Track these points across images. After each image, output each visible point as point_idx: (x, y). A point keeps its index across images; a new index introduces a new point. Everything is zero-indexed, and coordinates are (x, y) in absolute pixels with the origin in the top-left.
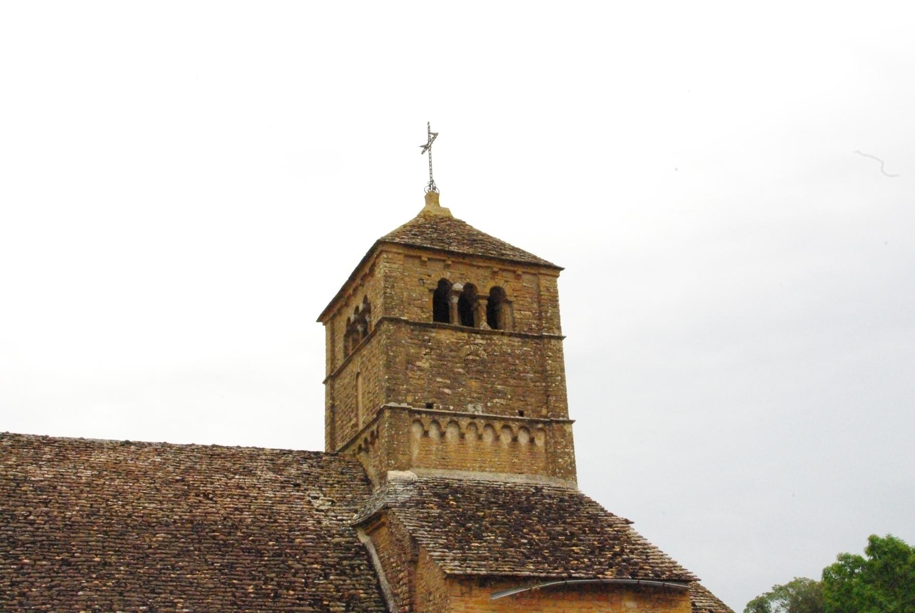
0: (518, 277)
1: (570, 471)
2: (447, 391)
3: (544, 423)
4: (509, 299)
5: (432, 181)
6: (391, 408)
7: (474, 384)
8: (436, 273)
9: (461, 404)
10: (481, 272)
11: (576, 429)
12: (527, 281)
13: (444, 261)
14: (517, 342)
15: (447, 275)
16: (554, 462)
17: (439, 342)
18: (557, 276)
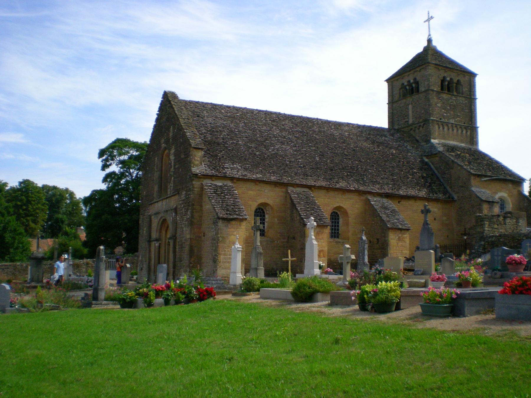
4: (462, 84)
5: (430, 35)
7: (452, 112)
8: (442, 74)
14: (464, 99)
15: (446, 75)
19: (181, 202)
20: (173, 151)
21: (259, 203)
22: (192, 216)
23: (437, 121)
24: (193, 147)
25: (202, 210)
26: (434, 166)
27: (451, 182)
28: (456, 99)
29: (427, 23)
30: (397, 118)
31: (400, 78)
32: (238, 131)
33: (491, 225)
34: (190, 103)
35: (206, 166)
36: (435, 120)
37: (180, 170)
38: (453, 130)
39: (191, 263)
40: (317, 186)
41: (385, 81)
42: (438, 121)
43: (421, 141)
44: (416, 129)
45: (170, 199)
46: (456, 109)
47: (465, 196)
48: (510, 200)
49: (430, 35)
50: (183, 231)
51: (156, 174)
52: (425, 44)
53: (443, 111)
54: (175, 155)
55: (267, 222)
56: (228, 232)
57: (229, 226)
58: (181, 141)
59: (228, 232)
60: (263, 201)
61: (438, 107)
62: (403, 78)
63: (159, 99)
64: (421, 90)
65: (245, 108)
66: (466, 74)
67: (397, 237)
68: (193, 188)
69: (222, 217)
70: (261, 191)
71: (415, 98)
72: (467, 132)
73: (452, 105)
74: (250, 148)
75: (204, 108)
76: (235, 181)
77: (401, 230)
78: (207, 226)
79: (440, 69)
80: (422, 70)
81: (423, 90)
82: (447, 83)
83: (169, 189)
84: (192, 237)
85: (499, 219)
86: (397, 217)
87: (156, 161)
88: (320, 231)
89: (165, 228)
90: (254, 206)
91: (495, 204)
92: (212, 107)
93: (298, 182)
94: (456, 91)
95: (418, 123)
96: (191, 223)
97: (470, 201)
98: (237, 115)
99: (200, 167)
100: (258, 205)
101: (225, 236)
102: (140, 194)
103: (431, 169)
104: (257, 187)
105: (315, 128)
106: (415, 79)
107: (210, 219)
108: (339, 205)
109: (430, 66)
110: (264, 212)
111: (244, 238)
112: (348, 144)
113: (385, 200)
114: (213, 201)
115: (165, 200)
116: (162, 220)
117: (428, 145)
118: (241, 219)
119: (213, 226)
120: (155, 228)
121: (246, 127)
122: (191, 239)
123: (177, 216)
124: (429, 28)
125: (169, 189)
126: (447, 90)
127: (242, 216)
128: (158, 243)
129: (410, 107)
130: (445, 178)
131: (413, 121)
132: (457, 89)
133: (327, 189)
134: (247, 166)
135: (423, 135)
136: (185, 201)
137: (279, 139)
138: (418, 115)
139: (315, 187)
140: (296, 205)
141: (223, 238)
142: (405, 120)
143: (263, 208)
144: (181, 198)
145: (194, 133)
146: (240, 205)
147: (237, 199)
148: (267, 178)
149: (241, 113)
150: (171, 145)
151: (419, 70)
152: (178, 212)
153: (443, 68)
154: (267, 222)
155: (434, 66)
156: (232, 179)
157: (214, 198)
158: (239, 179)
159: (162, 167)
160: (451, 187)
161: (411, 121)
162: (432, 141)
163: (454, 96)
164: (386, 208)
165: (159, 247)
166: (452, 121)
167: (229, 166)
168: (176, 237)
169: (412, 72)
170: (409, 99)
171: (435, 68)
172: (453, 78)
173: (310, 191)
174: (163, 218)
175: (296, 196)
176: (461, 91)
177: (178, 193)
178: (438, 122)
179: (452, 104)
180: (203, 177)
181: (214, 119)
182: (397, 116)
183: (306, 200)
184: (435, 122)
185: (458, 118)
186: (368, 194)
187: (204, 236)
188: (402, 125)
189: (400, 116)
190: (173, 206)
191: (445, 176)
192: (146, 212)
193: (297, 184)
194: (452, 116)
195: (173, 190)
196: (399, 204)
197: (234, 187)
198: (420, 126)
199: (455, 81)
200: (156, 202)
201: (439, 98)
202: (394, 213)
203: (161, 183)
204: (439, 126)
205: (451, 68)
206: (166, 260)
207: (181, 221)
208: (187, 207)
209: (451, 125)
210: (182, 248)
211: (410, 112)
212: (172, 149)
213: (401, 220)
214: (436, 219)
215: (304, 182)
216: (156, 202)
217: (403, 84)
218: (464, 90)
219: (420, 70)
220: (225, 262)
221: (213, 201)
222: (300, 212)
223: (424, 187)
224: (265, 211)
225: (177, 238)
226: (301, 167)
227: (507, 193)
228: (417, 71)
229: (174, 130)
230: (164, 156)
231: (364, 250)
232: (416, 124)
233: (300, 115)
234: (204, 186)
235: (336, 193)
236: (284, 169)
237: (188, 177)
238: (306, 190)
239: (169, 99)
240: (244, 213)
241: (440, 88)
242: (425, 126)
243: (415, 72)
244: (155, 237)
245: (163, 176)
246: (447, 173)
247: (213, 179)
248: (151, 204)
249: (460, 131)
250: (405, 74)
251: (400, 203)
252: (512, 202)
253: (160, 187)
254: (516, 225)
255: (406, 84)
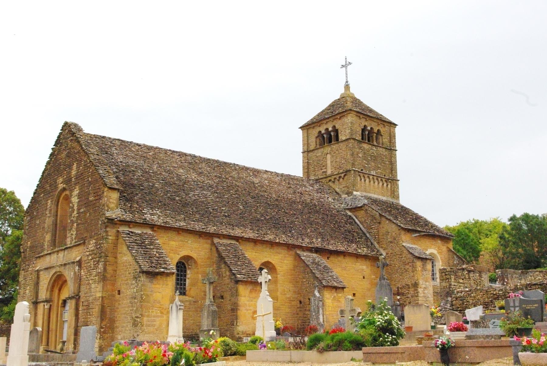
5: (347, 82)
7: (373, 164)
8: (364, 123)
15: (366, 124)
19: (88, 253)
20: (76, 192)
21: (182, 255)
23: (359, 172)
26: (359, 221)
29: (344, 69)
30: (313, 168)
31: (317, 125)
33: (456, 279)
35: (123, 210)
36: (357, 171)
37: (88, 215)
38: (374, 182)
42: (360, 172)
43: (341, 193)
45: (69, 250)
46: (377, 160)
47: (395, 253)
48: (439, 258)
49: (347, 82)
51: (49, 221)
52: (342, 91)
53: (364, 161)
54: (79, 196)
56: (153, 289)
60: (186, 254)
62: (320, 126)
63: (57, 131)
64: (342, 139)
65: (157, 147)
66: (386, 124)
70: (184, 241)
71: (334, 147)
73: (373, 156)
75: (112, 144)
76: (155, 229)
77: (336, 288)
79: (361, 117)
81: (344, 138)
82: (367, 133)
83: (70, 238)
84: (104, 295)
85: (463, 272)
86: (330, 274)
87: (49, 204)
89: (59, 286)
91: (428, 261)
92: (120, 144)
96: (103, 278)
97: (401, 258)
98: (150, 155)
99: (115, 211)
100: (181, 258)
101: (149, 293)
102: (21, 245)
103: (356, 223)
104: (181, 238)
105: (234, 173)
106: (334, 127)
107: (129, 273)
110: (185, 267)
112: (270, 193)
114: (134, 251)
115: (63, 252)
116: (55, 276)
118: (167, 273)
119: (134, 282)
120: (46, 286)
121: (161, 168)
123: (81, 270)
125: (70, 238)
126: (367, 140)
127: (169, 269)
128: (49, 305)
129: (329, 156)
130: (371, 232)
131: (332, 172)
132: (377, 139)
133: (255, 242)
134: (168, 212)
135: (343, 187)
136: (95, 252)
137: (199, 184)
138: (337, 165)
139: (243, 239)
140: (225, 258)
141: (147, 296)
142: (323, 171)
143: (184, 262)
145: (107, 172)
147: (160, 250)
148: (192, 227)
149: (154, 153)
151: (339, 118)
152: (83, 266)
153: (364, 117)
154: (188, 278)
155: (355, 113)
156: (152, 226)
157: (134, 248)
158: (160, 227)
159: (57, 212)
160: (378, 243)
161: (329, 172)
162: (355, 193)
163: (374, 147)
164: (318, 264)
165: (50, 309)
166: (373, 173)
167: (148, 211)
168: (80, 297)
169: (331, 119)
170: (327, 149)
172: (373, 128)
173: (238, 243)
174: (58, 273)
175: (224, 248)
176: (381, 142)
177: (84, 243)
178: (359, 174)
179: (372, 154)
180: (120, 223)
182: (312, 166)
183: (235, 253)
184: (357, 173)
185: (379, 170)
186: (298, 248)
187: (119, 294)
188: (319, 176)
189: (317, 166)
190: (76, 258)
191: (372, 231)
192: (31, 266)
194: (373, 168)
195: (75, 238)
196: (328, 260)
197: (155, 236)
198: (340, 177)
199: (376, 131)
202: (326, 270)
203: (56, 231)
205: (372, 117)
206: (58, 326)
207: (88, 276)
209: (372, 177)
211: (329, 162)
212: (75, 190)
213: (335, 278)
214: (365, 277)
215: (232, 233)
217: (320, 132)
218: (384, 141)
220: (149, 326)
221: (134, 251)
222: (231, 267)
224: (187, 266)
226: (226, 216)
228: (337, 118)
230: (61, 198)
231: (318, 308)
233: (216, 159)
234: (122, 233)
236: (208, 217)
237: (100, 223)
238: (233, 242)
241: (361, 138)
242: (346, 177)
243: (334, 120)
244: (44, 297)
248: (39, 257)
249: (381, 184)
252: (442, 259)
253: (54, 236)
254: (479, 279)
255: (323, 132)
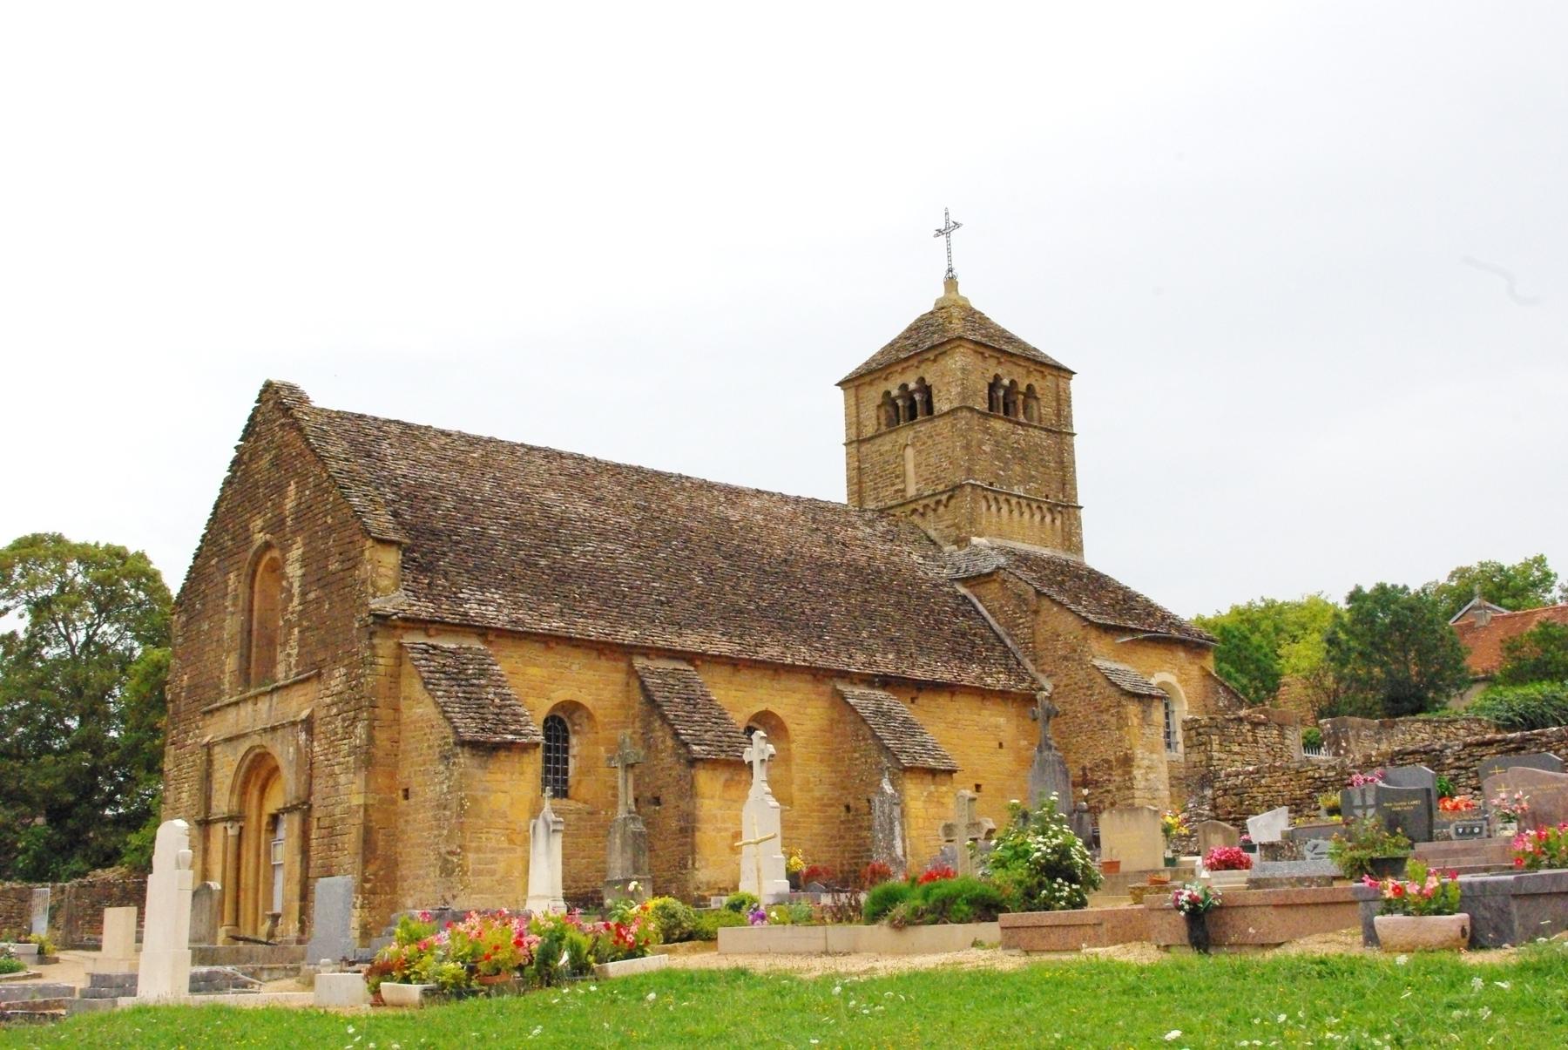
0: (1044, 377)
1: (1079, 549)
2: (1001, 473)
3: (1063, 506)
4: (1039, 396)
5: (950, 270)
6: (972, 485)
7: (1018, 468)
8: (993, 369)
9: (1010, 486)
10: (1020, 370)
11: (1083, 514)
12: (1050, 381)
13: (998, 358)
14: (1043, 434)
15: (999, 371)
16: (1069, 540)
17: (995, 430)
18: (1070, 379)
19: (328, 700)
20: (296, 552)
22: (371, 739)
23: (984, 489)
24: (373, 538)
25: (397, 721)
26: (986, 607)
27: (1034, 648)
28: (1026, 435)
32: (481, 501)
34: (342, 418)
35: (411, 594)
36: (979, 486)
37: (327, 607)
38: (1022, 514)
39: (366, 880)
40: (709, 655)
41: (838, 385)
42: (987, 489)
43: (941, 543)
44: (929, 510)
47: (1076, 684)
49: (950, 270)
50: (337, 784)
51: (232, 625)
52: (940, 292)
54: (305, 561)
55: (574, 756)
56: (488, 784)
57: (491, 767)
58: (330, 521)
59: (488, 784)
60: (568, 697)
61: (985, 453)
65: (490, 438)
67: (925, 794)
68: (375, 655)
69: (472, 739)
71: (922, 429)
72: (1053, 520)
74: (519, 547)
78: (418, 769)
80: (940, 357)
81: (946, 408)
82: (1001, 393)
86: (918, 738)
87: (231, 582)
88: (732, 779)
89: (260, 783)
90: (544, 708)
91: (1156, 702)
93: (660, 644)
94: (1025, 413)
95: (934, 495)
96: (367, 760)
97: (1091, 695)
98: (474, 458)
100: (556, 707)
101: (480, 794)
103: (978, 613)
104: (552, 658)
106: (922, 380)
107: (430, 747)
108: (764, 709)
109: (964, 347)
110: (566, 730)
111: (532, 800)
113: (880, 694)
114: (439, 693)
116: (251, 756)
117: (961, 552)
119: (442, 768)
122: (366, 807)
123: (312, 741)
124: (949, 251)
125: (283, 664)
128: (237, 826)
130: (1017, 635)
131: (918, 490)
133: (734, 663)
134: (521, 595)
144: (328, 689)
145: (371, 500)
146: (514, 705)
147: (503, 688)
150: (289, 536)
151: (932, 358)
152: (316, 731)
154: (574, 756)
158: (501, 633)
160: (1034, 661)
161: (911, 491)
162: (975, 540)
165: (240, 837)
166: (1018, 490)
169: (914, 362)
170: (906, 435)
171: (976, 352)
173: (692, 668)
174: (258, 751)
175: (659, 681)
177: (319, 675)
179: (1015, 445)
181: (414, 466)
184: (979, 491)
187: (406, 797)
193: (658, 649)
194: (1018, 478)
195: (297, 665)
196: (912, 706)
197: (491, 655)
198: (938, 502)
199: (1022, 388)
200: (229, 705)
201: (986, 431)
203: (249, 649)
204: (988, 501)
205: (1012, 355)
207: (330, 756)
208: (352, 713)
210: (331, 835)
211: (910, 467)
212: (295, 546)
213: (930, 747)
214: (1004, 744)
215: (678, 643)
216: (229, 705)
217: (888, 393)
219: (936, 356)
221: (439, 693)
223: (970, 660)
224: (569, 726)
225: (315, 806)
227: (1174, 674)
229: (300, 492)
230: (261, 569)
231: (891, 823)
232: (925, 497)
235: (758, 674)
238: (682, 666)
239: (282, 403)
240: (531, 728)
241: (987, 406)
242: (953, 502)
245: (255, 626)
246: (1023, 623)
247: (432, 632)
248: (211, 712)
250: (895, 369)
251: (916, 701)
252: (1188, 698)
